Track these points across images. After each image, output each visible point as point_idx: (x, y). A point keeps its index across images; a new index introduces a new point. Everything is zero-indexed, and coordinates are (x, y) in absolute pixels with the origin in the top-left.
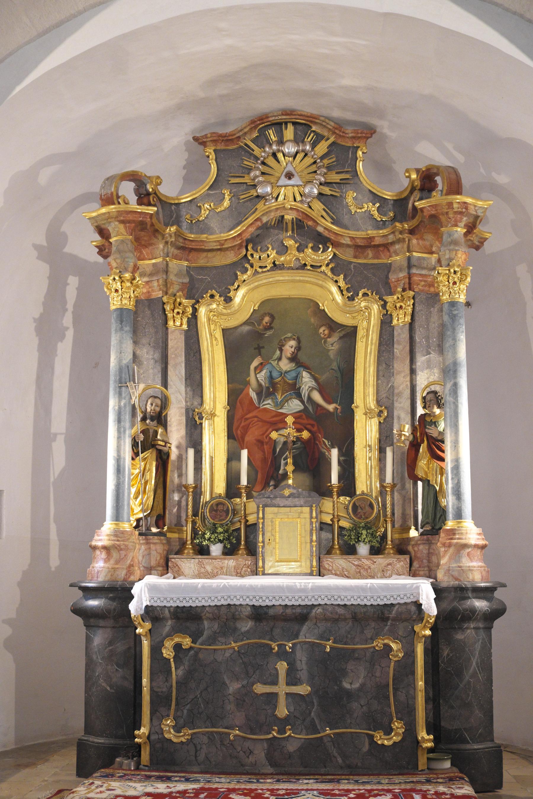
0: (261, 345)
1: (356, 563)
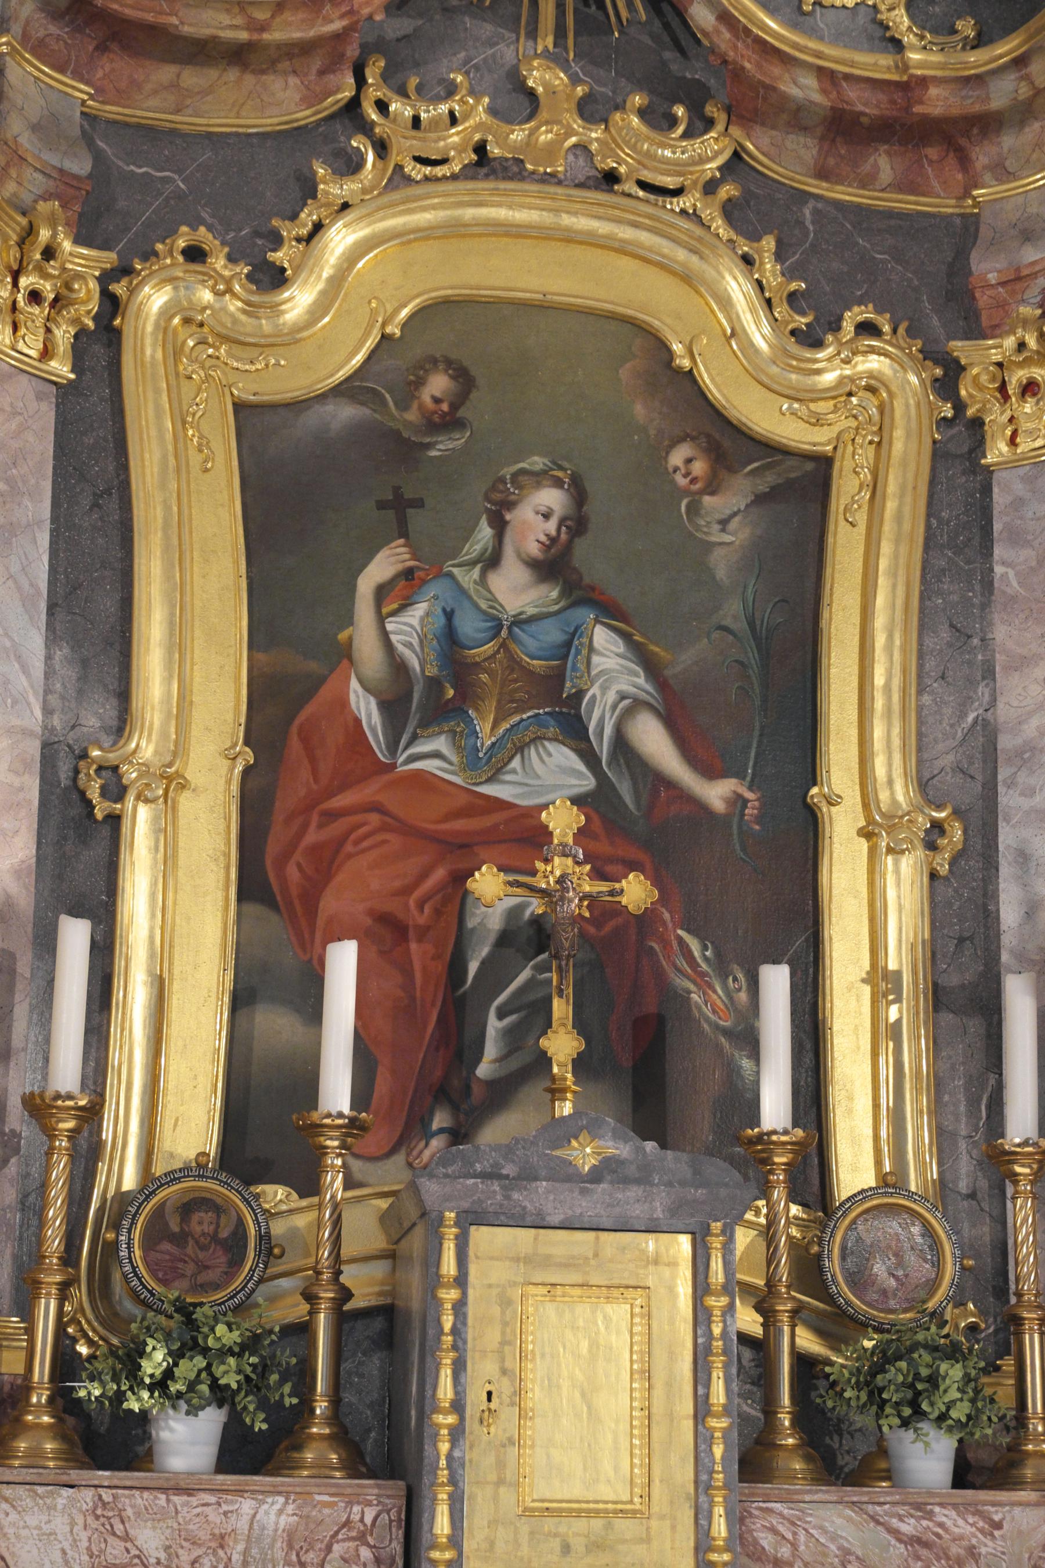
0: (408, 495)
1: (907, 1528)
